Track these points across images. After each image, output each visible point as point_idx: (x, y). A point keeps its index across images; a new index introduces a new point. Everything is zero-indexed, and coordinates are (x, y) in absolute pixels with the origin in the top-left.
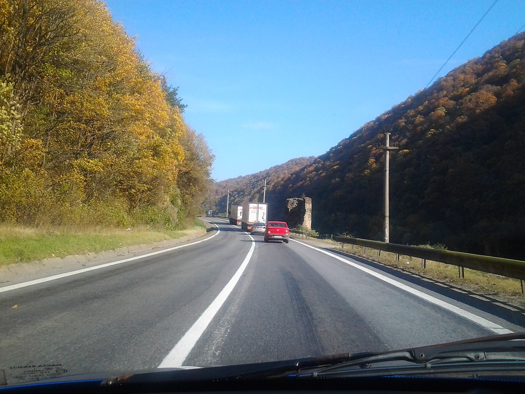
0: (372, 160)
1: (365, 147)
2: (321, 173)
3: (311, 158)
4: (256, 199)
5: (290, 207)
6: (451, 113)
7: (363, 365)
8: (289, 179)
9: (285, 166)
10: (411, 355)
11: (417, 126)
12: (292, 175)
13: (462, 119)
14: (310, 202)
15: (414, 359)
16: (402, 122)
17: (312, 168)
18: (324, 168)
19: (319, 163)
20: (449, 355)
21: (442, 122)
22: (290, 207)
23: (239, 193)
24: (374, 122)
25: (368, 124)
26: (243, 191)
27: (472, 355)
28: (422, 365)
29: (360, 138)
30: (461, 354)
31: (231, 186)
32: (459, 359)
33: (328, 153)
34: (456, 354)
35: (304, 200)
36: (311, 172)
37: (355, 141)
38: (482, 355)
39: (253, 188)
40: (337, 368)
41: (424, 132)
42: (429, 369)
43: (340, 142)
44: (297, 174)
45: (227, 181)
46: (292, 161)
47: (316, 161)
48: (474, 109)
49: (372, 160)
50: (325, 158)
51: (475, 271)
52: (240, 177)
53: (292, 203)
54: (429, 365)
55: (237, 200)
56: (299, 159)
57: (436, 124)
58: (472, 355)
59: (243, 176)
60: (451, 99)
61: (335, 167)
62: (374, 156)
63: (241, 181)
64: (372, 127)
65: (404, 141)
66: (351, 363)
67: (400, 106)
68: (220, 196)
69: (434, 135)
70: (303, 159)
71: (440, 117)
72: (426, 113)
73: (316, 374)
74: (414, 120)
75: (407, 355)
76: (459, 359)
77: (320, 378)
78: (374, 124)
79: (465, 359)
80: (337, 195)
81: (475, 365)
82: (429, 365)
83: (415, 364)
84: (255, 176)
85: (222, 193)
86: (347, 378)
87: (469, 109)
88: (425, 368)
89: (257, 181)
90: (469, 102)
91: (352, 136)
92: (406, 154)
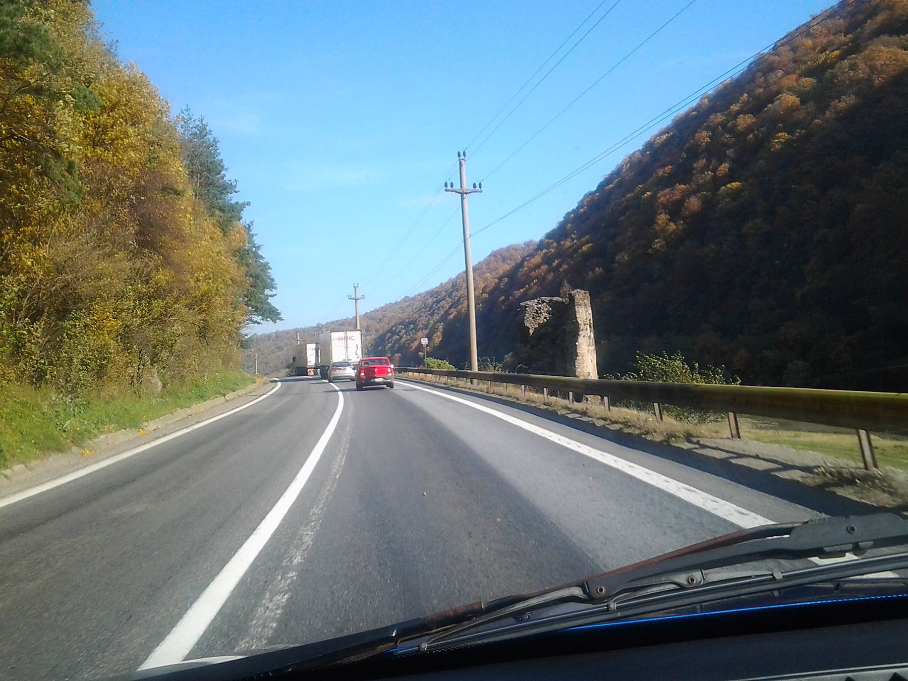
0: (662, 218)
1: (637, 198)
2: (560, 265)
3: (527, 244)
4: (439, 333)
5: (531, 325)
6: (819, 97)
7: (518, 615)
8: (497, 288)
9: (484, 268)
10: (584, 591)
11: (745, 133)
12: (500, 279)
13: (845, 103)
14: (587, 301)
15: (590, 599)
16: (704, 137)
17: (537, 259)
18: (561, 254)
19: (547, 246)
20: (646, 582)
21: (801, 115)
22: (531, 325)
23: (406, 326)
24: (643, 152)
25: (630, 158)
26: (414, 322)
27: (682, 579)
28: (602, 607)
29: (620, 185)
30: (664, 579)
31: (393, 317)
32: (662, 588)
33: (562, 226)
34: (654, 580)
35: (572, 298)
36: (538, 266)
37: (611, 192)
38: (697, 575)
39: (432, 315)
40: (490, 621)
41: (761, 144)
42: (614, 612)
43: (582, 201)
44: (512, 275)
45: (383, 309)
46: (494, 255)
47: (541, 246)
48: (869, 80)
49: (662, 218)
50: (559, 234)
51: (632, 464)
52: (406, 299)
53: (536, 314)
54: (613, 606)
55: (403, 340)
56: (508, 249)
57: (787, 120)
58: (682, 579)
59: (411, 296)
60: (809, 73)
61: (584, 248)
62: (664, 208)
63: (408, 306)
64: (640, 161)
65: (724, 167)
66: (484, 619)
67: (687, 115)
68: (373, 337)
69: (788, 144)
70: (514, 248)
71: (791, 110)
72: (756, 107)
73: (425, 646)
74: (735, 125)
75: (577, 592)
76: (662, 588)
77: (431, 652)
78: (642, 155)
79: (672, 586)
80: (499, 332)
81: (686, 594)
82: (613, 606)
83: (591, 606)
84: (431, 293)
85: (377, 331)
86: (478, 646)
87: (853, 82)
88: (608, 610)
89: (438, 302)
90: (855, 69)
91: (601, 187)
92: (736, 194)
